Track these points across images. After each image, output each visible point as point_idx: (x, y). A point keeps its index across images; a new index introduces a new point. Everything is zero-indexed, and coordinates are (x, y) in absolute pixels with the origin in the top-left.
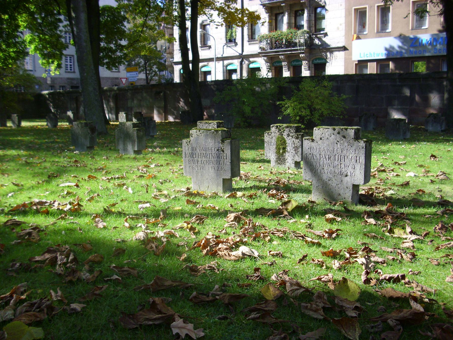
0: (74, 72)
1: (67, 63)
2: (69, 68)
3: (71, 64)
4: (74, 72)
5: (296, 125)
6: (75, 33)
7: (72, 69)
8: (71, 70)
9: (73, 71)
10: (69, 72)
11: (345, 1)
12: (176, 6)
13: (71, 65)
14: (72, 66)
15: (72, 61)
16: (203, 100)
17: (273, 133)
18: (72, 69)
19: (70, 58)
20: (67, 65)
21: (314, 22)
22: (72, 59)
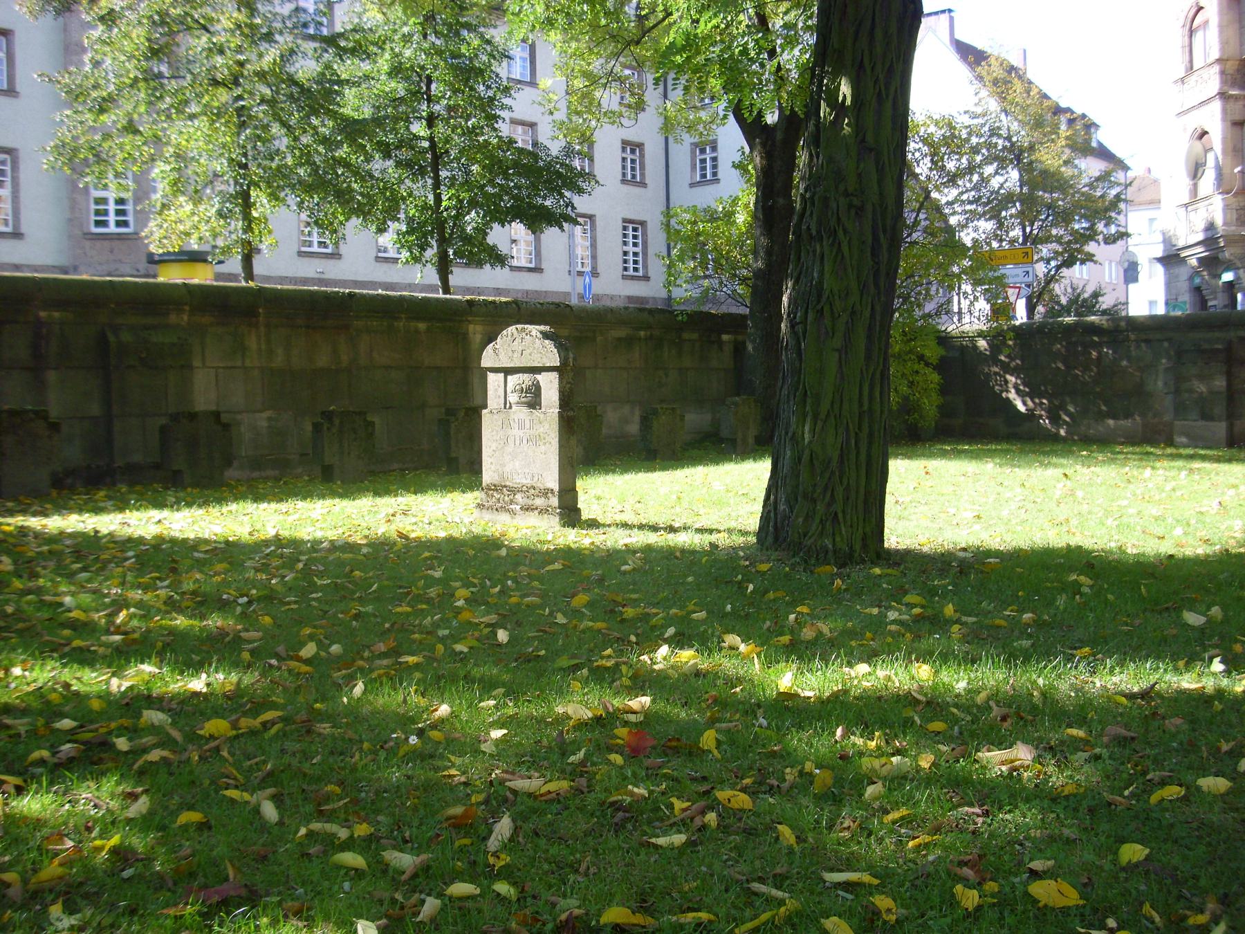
0: (646, 278)
1: (625, 248)
2: (631, 265)
3: (636, 250)
4: (646, 278)
5: (1120, 679)
6: (799, 185)
7: (640, 266)
8: (636, 270)
9: (640, 273)
10: (632, 278)
11: (1220, 4)
12: (127, 35)
13: (635, 254)
14: (640, 259)
15: (640, 241)
16: (1223, 389)
17: (529, 899)
18: (640, 266)
19: (635, 230)
20: (625, 253)
21: (877, 20)
22: (639, 233)
